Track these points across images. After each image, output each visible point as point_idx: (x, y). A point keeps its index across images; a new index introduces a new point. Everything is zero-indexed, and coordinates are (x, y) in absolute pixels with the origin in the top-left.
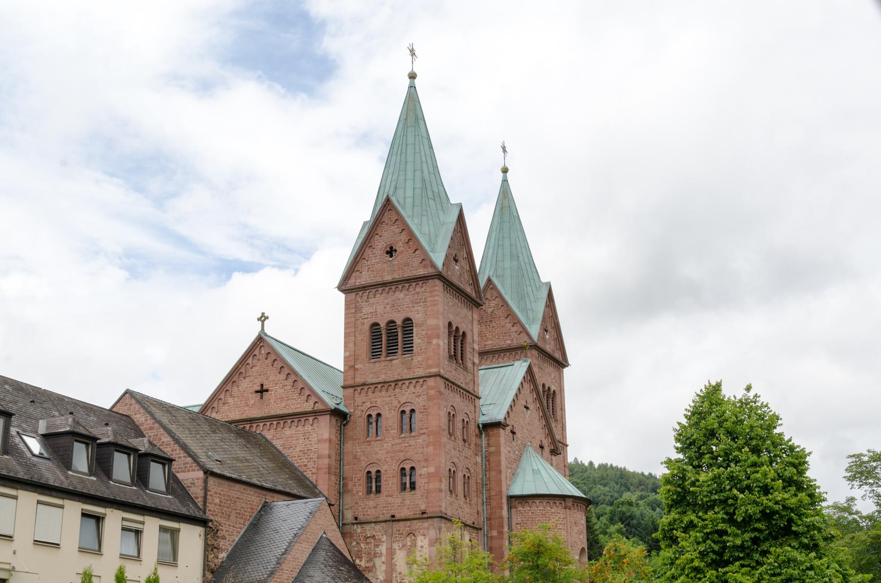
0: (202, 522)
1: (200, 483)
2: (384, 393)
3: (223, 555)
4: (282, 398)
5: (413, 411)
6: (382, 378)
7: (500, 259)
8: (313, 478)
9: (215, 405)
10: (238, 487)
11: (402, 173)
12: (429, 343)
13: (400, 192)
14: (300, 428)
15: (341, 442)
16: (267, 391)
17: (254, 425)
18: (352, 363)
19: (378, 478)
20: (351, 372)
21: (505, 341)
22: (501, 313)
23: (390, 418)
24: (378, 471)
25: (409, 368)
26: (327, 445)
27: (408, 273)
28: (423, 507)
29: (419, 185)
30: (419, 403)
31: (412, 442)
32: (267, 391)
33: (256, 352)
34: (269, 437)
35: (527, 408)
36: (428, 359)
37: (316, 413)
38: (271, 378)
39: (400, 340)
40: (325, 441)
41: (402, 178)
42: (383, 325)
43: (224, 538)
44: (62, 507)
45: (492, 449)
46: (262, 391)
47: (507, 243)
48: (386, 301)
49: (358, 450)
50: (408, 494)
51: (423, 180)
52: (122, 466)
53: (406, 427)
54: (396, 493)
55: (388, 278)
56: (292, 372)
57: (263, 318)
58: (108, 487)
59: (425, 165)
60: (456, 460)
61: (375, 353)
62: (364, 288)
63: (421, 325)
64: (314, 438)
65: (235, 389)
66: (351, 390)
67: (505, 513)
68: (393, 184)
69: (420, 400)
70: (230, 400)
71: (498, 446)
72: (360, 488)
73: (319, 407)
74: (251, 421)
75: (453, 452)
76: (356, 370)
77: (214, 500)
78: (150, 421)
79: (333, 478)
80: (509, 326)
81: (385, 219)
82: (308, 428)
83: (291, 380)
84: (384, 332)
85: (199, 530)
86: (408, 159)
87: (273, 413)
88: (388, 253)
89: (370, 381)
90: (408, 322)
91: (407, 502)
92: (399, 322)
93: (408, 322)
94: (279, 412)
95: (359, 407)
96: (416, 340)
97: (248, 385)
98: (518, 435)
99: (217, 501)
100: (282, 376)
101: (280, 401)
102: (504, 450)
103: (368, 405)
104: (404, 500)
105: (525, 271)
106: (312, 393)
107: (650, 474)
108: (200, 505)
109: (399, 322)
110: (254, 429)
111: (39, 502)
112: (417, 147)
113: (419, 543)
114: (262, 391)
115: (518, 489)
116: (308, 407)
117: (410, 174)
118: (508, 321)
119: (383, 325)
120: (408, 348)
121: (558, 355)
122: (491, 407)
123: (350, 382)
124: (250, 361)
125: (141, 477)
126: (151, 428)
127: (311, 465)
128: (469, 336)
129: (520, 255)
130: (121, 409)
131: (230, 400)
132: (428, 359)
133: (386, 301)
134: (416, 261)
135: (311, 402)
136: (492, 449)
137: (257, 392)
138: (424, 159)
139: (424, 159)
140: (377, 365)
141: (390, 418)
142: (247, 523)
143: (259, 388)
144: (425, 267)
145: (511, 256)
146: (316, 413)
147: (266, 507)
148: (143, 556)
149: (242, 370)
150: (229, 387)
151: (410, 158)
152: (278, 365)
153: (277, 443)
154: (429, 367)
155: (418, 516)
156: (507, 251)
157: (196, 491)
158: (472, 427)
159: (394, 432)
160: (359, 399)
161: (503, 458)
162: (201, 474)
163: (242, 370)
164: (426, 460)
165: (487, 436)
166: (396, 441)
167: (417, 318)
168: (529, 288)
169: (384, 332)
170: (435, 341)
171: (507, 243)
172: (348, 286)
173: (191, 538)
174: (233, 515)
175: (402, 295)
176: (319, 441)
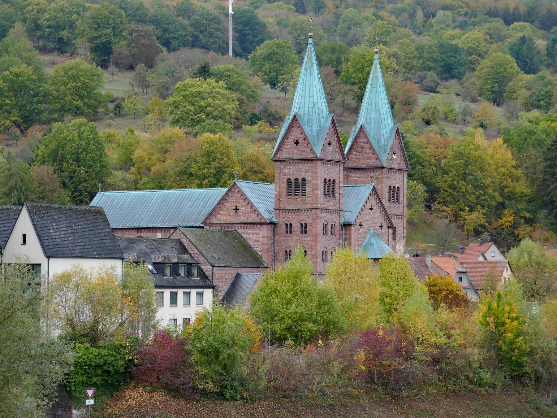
0: (213, 287)
1: (210, 270)
2: (293, 214)
7: (369, 112)
8: (260, 254)
9: (214, 214)
10: (225, 269)
11: (303, 98)
12: (313, 192)
14: (254, 229)
15: (274, 235)
16: (238, 209)
18: (278, 198)
19: (306, 227)
20: (278, 202)
21: (369, 162)
22: (367, 146)
23: (296, 227)
24: (290, 251)
26: (266, 239)
29: (311, 106)
30: (308, 221)
31: (305, 239)
32: (238, 209)
33: (233, 190)
34: (240, 232)
36: (313, 200)
37: (261, 224)
38: (240, 204)
39: (300, 188)
40: (265, 237)
41: (303, 101)
42: (293, 180)
43: (221, 291)
45: (348, 236)
47: (374, 102)
48: (294, 168)
49: (282, 240)
51: (314, 102)
52: (182, 271)
55: (295, 157)
56: (249, 202)
58: (178, 280)
59: (315, 93)
60: (327, 246)
61: (289, 194)
62: (284, 160)
63: (310, 183)
65: (224, 207)
66: (278, 211)
68: (299, 104)
69: (308, 219)
70: (221, 212)
71: (350, 235)
72: (282, 258)
73: (262, 221)
74: (232, 224)
75: (325, 242)
76: (280, 201)
77: (216, 276)
78: (189, 243)
79: (270, 254)
80: (371, 154)
81: (294, 125)
82: (258, 230)
83: (249, 206)
84: (293, 184)
85: (210, 291)
86: (307, 90)
88: (295, 143)
90: (304, 180)
92: (300, 180)
94: (245, 221)
95: (282, 220)
96: (308, 190)
99: (217, 277)
100: (245, 203)
101: (245, 216)
103: (286, 219)
105: (383, 120)
106: (259, 214)
108: (211, 279)
109: (300, 180)
112: (311, 82)
116: (257, 220)
117: (307, 100)
118: (371, 151)
119: (293, 180)
120: (304, 193)
122: (350, 213)
123: (278, 207)
124: (230, 194)
125: (189, 274)
126: (189, 245)
127: (259, 247)
128: (337, 182)
129: (381, 110)
131: (221, 212)
132: (313, 200)
133: (294, 168)
134: (308, 150)
135: (259, 218)
136: (348, 236)
137: (234, 209)
138: (315, 89)
139: (315, 89)
140: (290, 200)
141: (296, 227)
142: (230, 283)
143: (235, 208)
144: (312, 153)
145: (376, 110)
146: (261, 224)
147: (238, 276)
149: (227, 198)
150: (220, 205)
151: (307, 89)
152: (243, 197)
153: (244, 236)
154: (313, 204)
156: (373, 107)
157: (209, 274)
158: (338, 226)
160: (282, 215)
162: (211, 267)
163: (227, 198)
164: (311, 248)
165: (346, 229)
166: (298, 238)
167: (308, 179)
168: (385, 130)
169: (293, 184)
170: (316, 192)
171: (374, 102)
172: (276, 159)
173: (208, 294)
174: (224, 280)
175: (301, 166)
176: (263, 237)
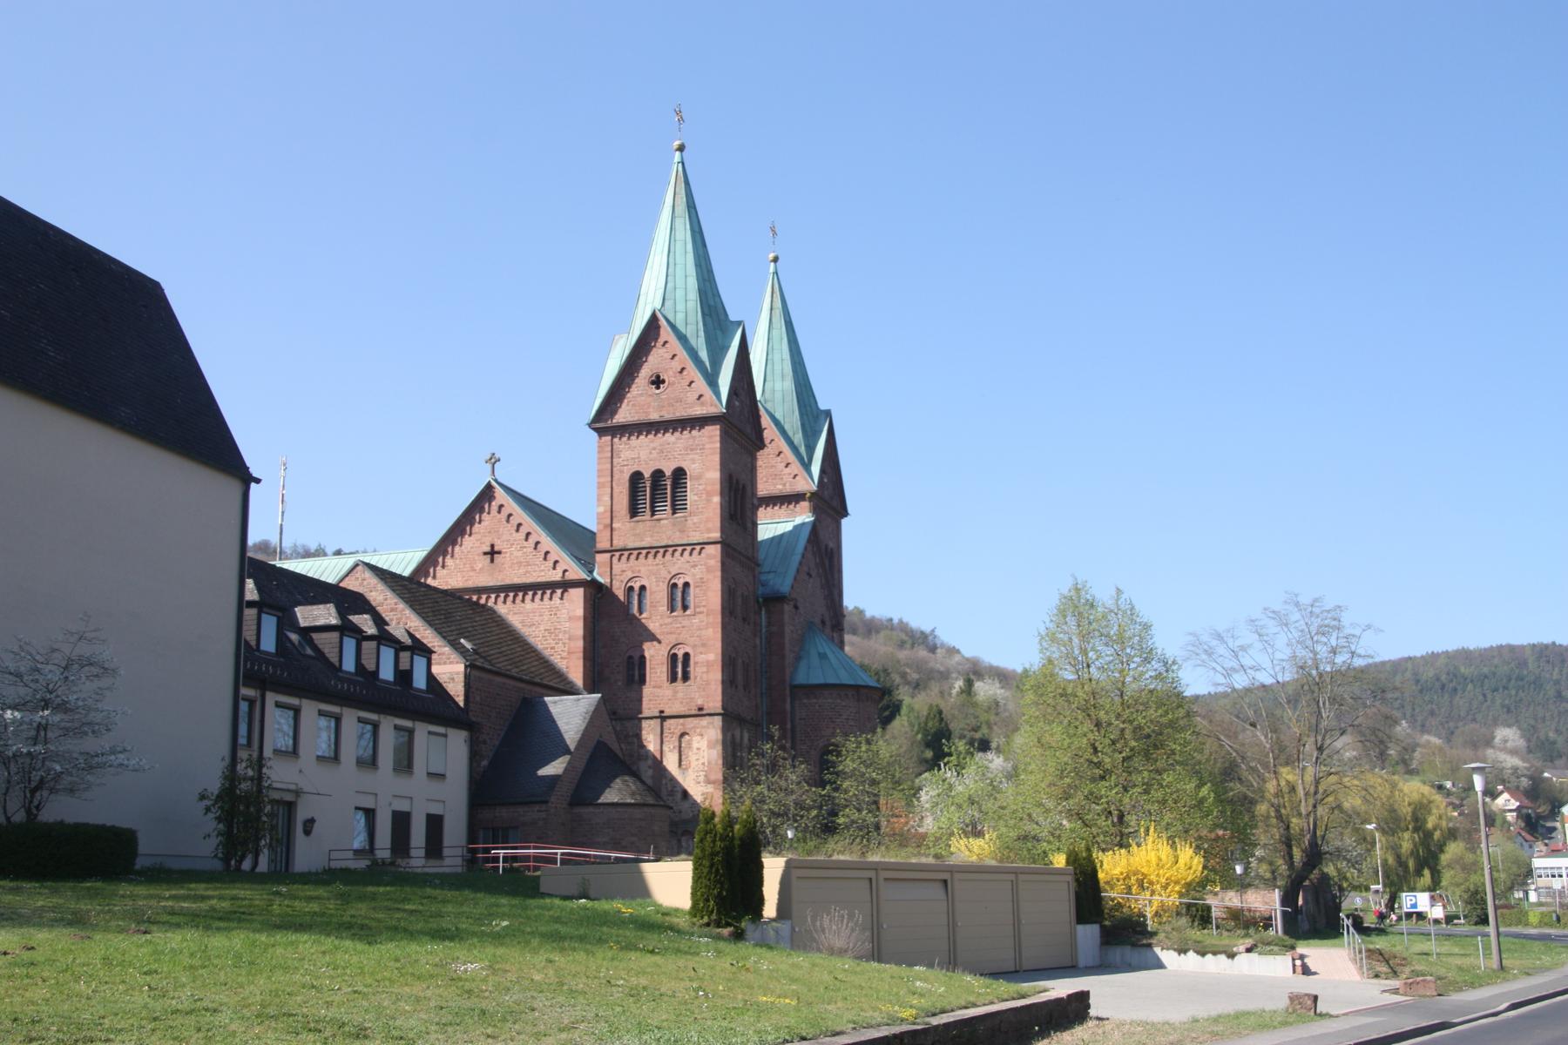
3: (485, 763)
4: (520, 563)
5: (686, 585)
6: (646, 542)
13: (668, 304)
17: (484, 597)
25: (682, 531)
27: (681, 413)
28: (700, 702)
31: (686, 622)
35: (810, 575)
43: (485, 742)
44: (445, 736)
46: (492, 553)
50: (679, 684)
53: (679, 604)
54: (666, 684)
55: (654, 416)
57: (493, 461)
63: (699, 477)
64: (564, 614)
67: (788, 707)
74: (480, 591)
87: (508, 582)
88: (653, 383)
89: (631, 545)
90: (679, 473)
91: (680, 695)
92: (668, 473)
93: (679, 473)
94: (517, 581)
96: (691, 497)
97: (472, 545)
98: (802, 610)
102: (788, 629)
104: (676, 692)
107: (901, 621)
109: (668, 473)
110: (483, 601)
111: (430, 733)
113: (695, 745)
114: (492, 553)
115: (802, 678)
121: (835, 503)
130: (350, 584)
148: (302, 751)
155: (694, 712)
159: (664, 608)
161: (787, 641)
